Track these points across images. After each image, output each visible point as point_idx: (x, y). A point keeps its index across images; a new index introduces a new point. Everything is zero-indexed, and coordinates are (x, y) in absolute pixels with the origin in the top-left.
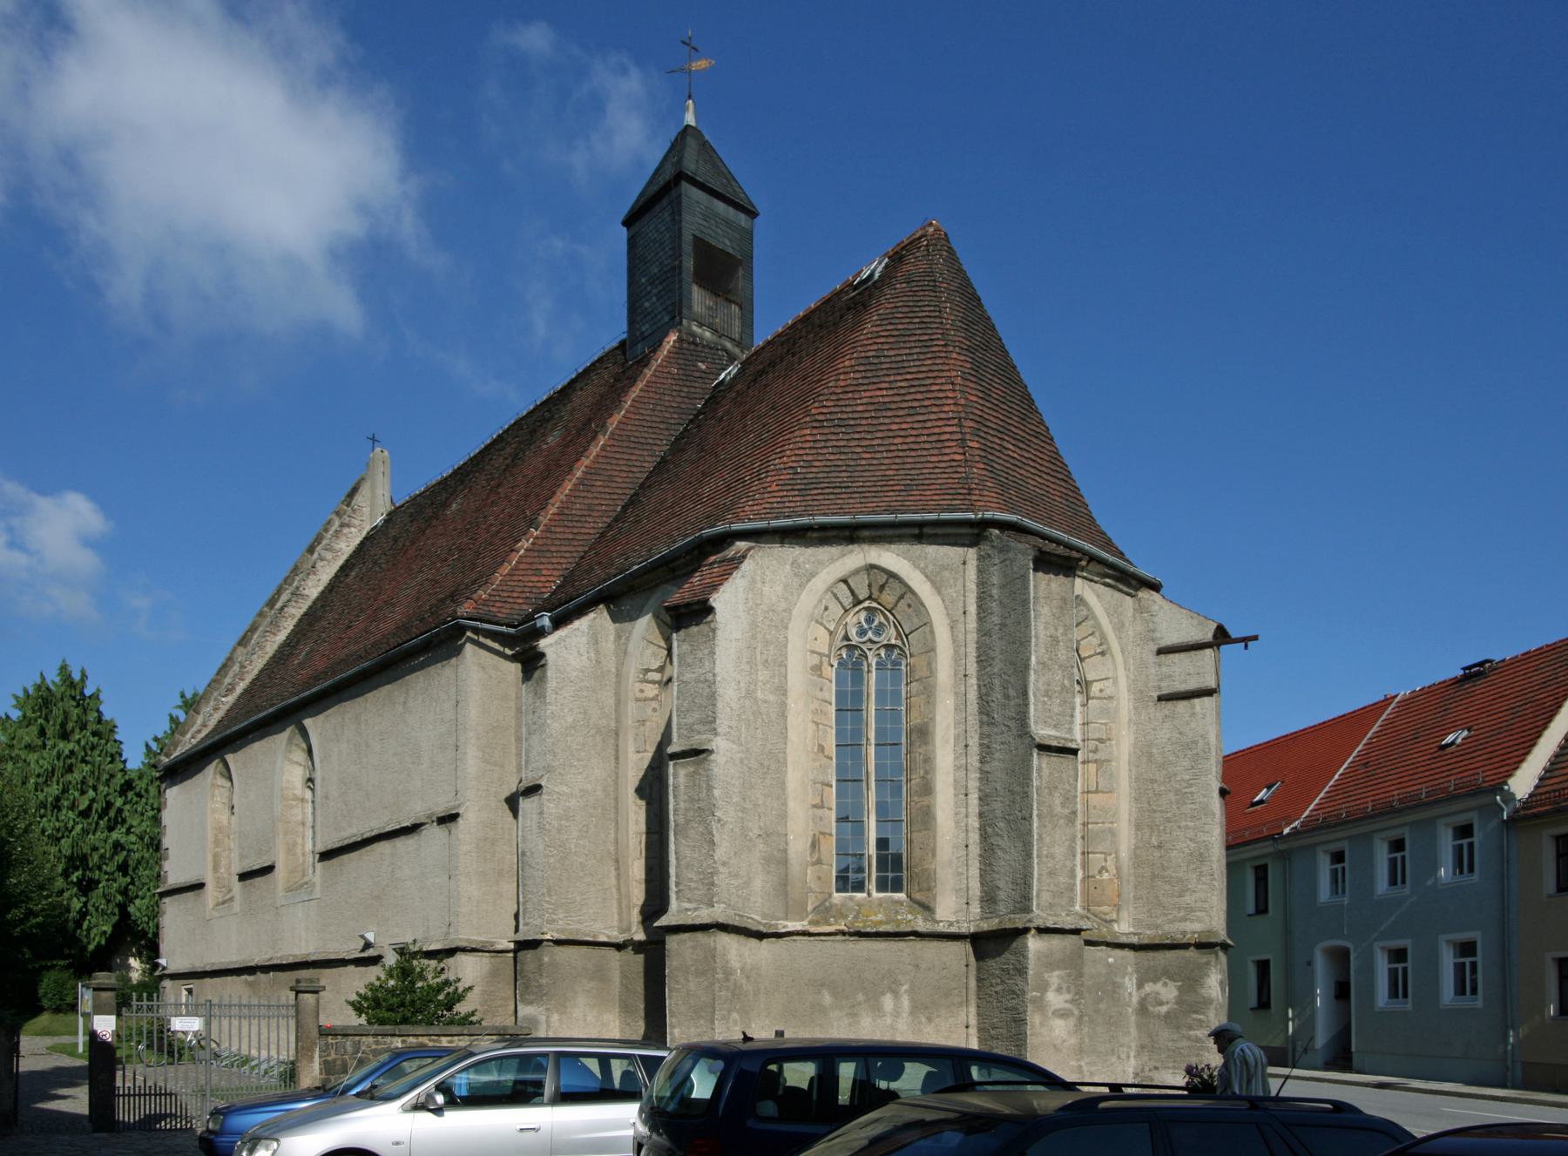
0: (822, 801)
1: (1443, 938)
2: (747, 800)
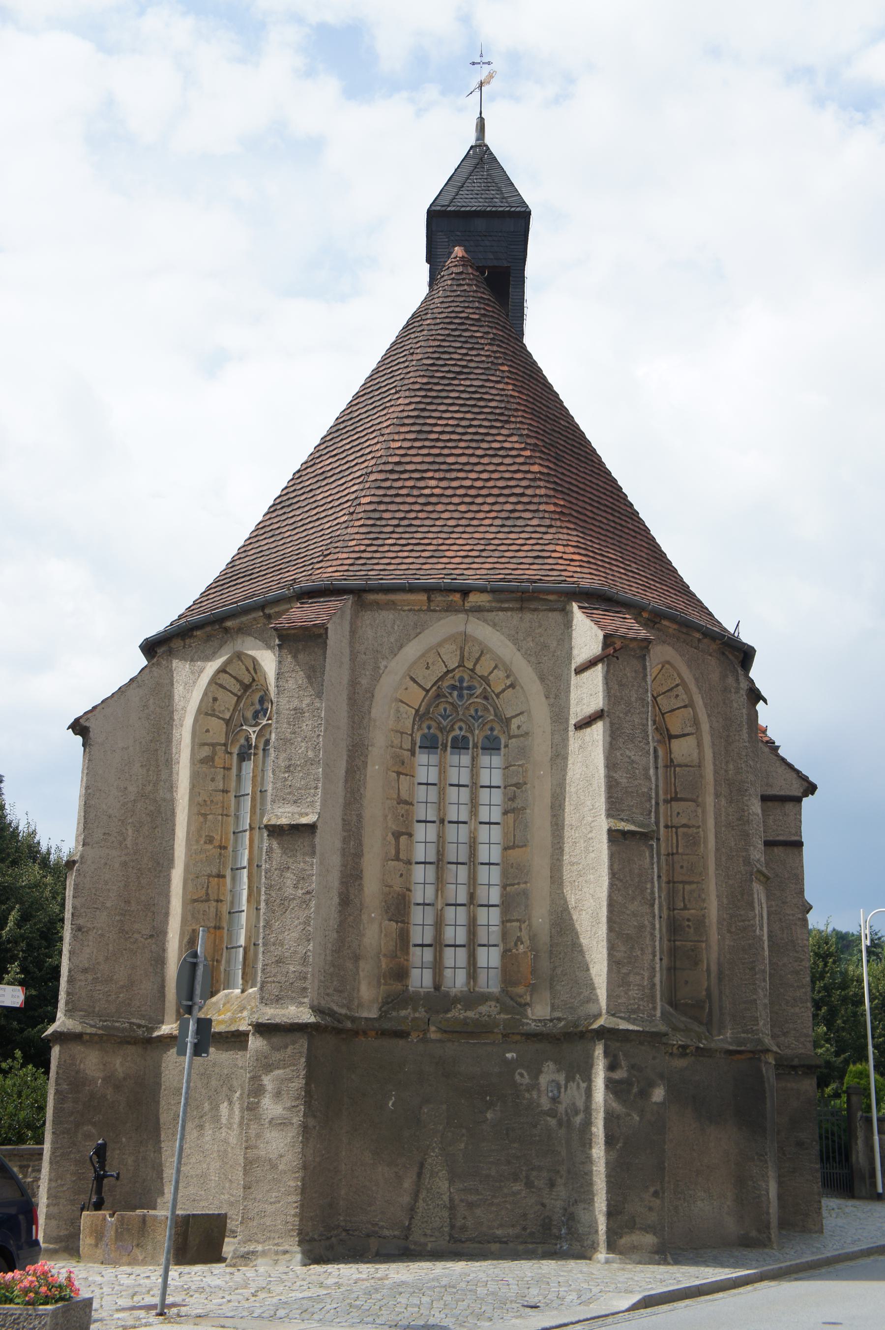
0: (207, 894)
1: (515, 1055)
2: (590, 836)
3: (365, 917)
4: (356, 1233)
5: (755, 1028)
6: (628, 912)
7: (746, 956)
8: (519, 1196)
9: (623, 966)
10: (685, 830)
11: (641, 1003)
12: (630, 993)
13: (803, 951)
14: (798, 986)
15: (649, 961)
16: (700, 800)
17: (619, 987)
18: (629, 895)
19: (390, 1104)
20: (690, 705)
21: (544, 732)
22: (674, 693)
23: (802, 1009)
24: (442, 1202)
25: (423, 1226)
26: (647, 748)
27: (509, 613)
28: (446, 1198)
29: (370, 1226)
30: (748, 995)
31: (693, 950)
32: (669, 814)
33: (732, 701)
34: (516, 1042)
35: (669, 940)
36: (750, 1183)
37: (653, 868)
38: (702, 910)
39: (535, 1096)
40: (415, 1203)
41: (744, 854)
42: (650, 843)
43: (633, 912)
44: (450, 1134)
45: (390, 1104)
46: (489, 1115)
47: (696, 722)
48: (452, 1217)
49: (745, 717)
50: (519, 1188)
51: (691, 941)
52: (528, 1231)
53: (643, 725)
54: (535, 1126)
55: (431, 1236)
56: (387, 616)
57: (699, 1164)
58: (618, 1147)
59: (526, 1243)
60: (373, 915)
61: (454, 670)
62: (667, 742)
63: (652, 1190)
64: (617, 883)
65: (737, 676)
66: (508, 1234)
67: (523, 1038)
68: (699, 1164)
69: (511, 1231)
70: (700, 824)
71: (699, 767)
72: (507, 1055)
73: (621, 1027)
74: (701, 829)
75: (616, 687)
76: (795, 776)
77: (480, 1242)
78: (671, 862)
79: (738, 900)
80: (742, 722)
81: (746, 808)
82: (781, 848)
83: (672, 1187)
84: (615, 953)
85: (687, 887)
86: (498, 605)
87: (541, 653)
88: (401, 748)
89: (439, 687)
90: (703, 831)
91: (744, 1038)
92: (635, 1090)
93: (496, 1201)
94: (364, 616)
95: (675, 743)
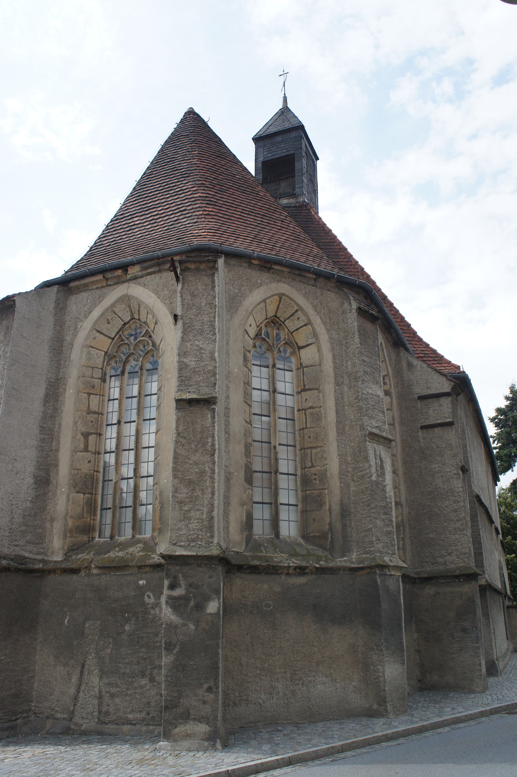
3: (58, 492)
4: (41, 715)
5: (372, 549)
6: (191, 462)
7: (365, 497)
8: (145, 689)
9: (185, 505)
10: (311, 410)
11: (200, 533)
12: (190, 526)
13: (459, 495)
14: (457, 520)
15: (208, 499)
16: (321, 388)
17: (181, 521)
18: (192, 448)
19: (66, 622)
20: (309, 323)
21: (172, 348)
22: (296, 316)
23: (461, 535)
24: (94, 693)
25: (82, 711)
26: (214, 337)
27: (153, 276)
28: (97, 690)
29: (49, 711)
30: (366, 525)
31: (318, 496)
32: (300, 401)
33: (348, 319)
34: (146, 573)
35: (302, 491)
36: (372, 667)
37: (214, 426)
38: (324, 466)
39: (158, 612)
40: (78, 693)
41: (360, 423)
42: (212, 407)
43: (195, 462)
44: (102, 642)
45: (66, 622)
46: (127, 628)
47: (315, 335)
48: (100, 704)
49: (356, 327)
50: (145, 682)
51: (317, 490)
52: (151, 716)
53: (211, 322)
54: (157, 635)
55: (87, 718)
56: (84, 295)
57: (320, 656)
58: (175, 652)
59: (149, 725)
60: (63, 490)
61: (129, 322)
62: (298, 352)
63: (206, 686)
64: (181, 440)
65: (350, 301)
66: (137, 718)
67: (151, 569)
68: (320, 656)
69: (138, 715)
70: (322, 404)
71: (320, 365)
72: (140, 582)
73: (177, 553)
74: (322, 408)
75: (189, 298)
76: (445, 379)
77: (117, 724)
78: (302, 435)
79: (358, 457)
80: (354, 331)
81: (360, 390)
82: (439, 428)
83: (289, 675)
84: (178, 495)
85: (314, 451)
86: (144, 272)
87: (172, 297)
88: (92, 377)
89: (120, 335)
90: (324, 409)
91: (364, 558)
92: (192, 604)
93: (129, 692)
94: (71, 298)
95: (302, 351)
